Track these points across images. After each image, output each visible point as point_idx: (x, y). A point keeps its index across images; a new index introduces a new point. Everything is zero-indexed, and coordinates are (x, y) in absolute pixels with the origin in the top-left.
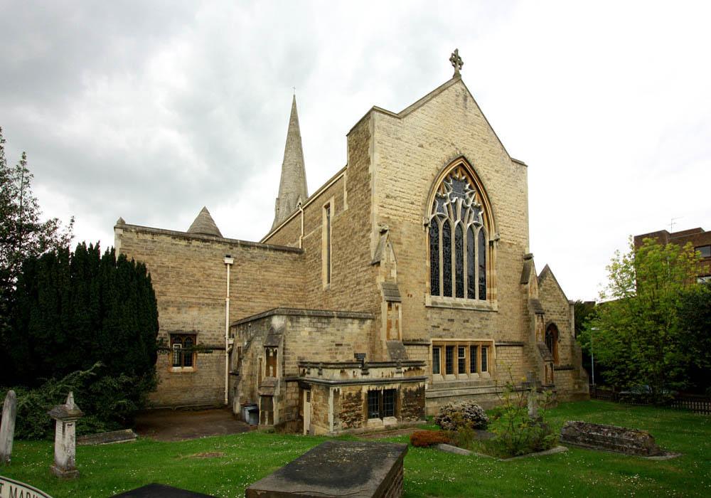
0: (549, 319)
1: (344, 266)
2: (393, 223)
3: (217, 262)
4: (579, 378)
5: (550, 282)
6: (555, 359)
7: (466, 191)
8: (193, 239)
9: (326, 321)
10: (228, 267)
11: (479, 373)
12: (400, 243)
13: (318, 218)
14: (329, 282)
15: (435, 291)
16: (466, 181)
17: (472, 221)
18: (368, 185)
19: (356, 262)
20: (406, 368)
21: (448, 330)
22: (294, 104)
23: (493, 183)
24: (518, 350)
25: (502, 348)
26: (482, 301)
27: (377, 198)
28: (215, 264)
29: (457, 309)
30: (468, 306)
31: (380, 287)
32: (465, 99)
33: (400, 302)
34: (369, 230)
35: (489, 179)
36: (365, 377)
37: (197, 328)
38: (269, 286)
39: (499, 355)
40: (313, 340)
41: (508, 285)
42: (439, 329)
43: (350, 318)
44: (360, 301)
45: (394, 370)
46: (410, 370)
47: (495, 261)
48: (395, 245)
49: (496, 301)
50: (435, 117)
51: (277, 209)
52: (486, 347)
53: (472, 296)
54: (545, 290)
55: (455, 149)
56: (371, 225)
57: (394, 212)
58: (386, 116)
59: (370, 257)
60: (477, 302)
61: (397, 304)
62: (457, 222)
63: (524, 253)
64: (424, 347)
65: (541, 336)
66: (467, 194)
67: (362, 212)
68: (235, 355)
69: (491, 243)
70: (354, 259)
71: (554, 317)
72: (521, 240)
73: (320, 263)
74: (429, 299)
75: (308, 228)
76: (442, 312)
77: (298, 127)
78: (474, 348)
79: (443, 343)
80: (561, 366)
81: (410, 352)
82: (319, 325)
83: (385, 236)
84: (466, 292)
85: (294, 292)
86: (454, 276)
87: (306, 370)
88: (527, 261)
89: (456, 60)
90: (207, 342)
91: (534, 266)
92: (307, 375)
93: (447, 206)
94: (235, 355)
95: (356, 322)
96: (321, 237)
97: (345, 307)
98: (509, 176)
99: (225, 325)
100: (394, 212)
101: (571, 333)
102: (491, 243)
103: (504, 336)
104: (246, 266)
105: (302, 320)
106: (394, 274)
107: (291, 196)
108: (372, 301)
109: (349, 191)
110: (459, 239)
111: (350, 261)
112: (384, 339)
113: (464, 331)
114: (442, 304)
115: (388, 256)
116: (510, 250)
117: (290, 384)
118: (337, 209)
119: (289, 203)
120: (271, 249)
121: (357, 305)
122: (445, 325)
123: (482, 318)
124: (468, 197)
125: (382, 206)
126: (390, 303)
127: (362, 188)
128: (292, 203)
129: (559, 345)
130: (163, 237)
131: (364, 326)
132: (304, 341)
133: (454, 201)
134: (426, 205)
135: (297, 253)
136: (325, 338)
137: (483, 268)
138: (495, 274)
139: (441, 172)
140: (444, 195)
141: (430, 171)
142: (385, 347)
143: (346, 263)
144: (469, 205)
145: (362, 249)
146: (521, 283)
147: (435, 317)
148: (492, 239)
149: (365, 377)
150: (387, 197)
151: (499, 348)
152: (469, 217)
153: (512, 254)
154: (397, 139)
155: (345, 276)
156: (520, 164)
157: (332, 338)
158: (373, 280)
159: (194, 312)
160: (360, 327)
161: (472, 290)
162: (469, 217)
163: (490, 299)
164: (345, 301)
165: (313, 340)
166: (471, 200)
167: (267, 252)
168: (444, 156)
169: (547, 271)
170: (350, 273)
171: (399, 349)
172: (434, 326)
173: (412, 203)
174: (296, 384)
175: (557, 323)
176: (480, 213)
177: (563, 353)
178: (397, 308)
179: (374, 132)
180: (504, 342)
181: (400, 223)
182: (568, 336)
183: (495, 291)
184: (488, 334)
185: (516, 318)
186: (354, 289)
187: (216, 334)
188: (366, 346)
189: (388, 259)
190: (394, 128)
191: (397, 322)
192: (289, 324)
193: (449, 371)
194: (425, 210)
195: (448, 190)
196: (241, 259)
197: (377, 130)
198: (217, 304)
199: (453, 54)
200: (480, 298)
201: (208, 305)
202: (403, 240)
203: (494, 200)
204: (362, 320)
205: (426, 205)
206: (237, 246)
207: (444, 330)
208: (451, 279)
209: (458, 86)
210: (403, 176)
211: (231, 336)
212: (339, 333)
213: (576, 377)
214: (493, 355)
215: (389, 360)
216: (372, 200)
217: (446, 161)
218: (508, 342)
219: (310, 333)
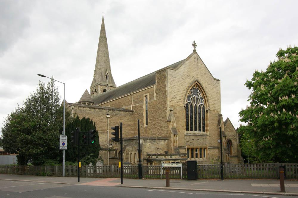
0: (228, 138)
1: (154, 120)
3: (104, 117)
4: (240, 160)
5: (229, 124)
6: (231, 153)
7: (198, 92)
8: (96, 108)
9: (154, 141)
10: (108, 118)
11: (203, 158)
12: (176, 114)
13: (141, 99)
14: (147, 124)
15: (187, 129)
16: (198, 89)
17: (200, 103)
18: (166, 94)
20: (182, 156)
21: (192, 143)
22: (103, 21)
23: (208, 89)
24: (217, 150)
25: (211, 149)
26: (203, 132)
27: (169, 98)
28: (104, 117)
29: (195, 135)
30: (199, 134)
31: (170, 129)
32: (198, 60)
33: (177, 134)
34: (166, 109)
35: (206, 88)
36: (171, 158)
39: (210, 152)
40: (150, 147)
41: (213, 126)
42: (189, 143)
43: (161, 139)
44: (162, 133)
45: (179, 156)
46: (183, 156)
47: (208, 117)
48: (175, 115)
49: (208, 132)
52: (205, 149)
53: (200, 130)
54: (227, 127)
55: (194, 78)
56: (167, 108)
57: (174, 103)
58: (171, 70)
59: (166, 118)
60: (202, 132)
61: (176, 135)
63: (219, 114)
64: (184, 149)
65: (225, 145)
66: (198, 93)
67: (163, 102)
69: (207, 111)
70: (159, 118)
71: (230, 137)
72: (218, 109)
74: (186, 132)
75: (136, 101)
76: (190, 137)
77: (105, 33)
78: (201, 149)
79: (190, 148)
80: (233, 156)
81: (181, 150)
82: (152, 142)
83: (172, 112)
84: (198, 129)
85: (130, 127)
86: (194, 123)
87: (150, 156)
88: (220, 117)
89: (194, 45)
91: (222, 119)
92: (151, 158)
93: (191, 99)
95: (163, 141)
96: (143, 107)
97: (155, 135)
98: (213, 86)
99: (107, 140)
100: (174, 103)
101: (237, 143)
102: (207, 111)
103: (212, 145)
104: (114, 118)
105: (147, 140)
106: (175, 124)
107: (103, 70)
109: (157, 94)
110: (196, 110)
111: (157, 118)
112: (172, 147)
113: (197, 143)
114: (189, 134)
115: (173, 119)
116: (214, 113)
117: (144, 161)
118: (150, 99)
120: (122, 111)
121: (161, 134)
122: (191, 141)
123: (204, 138)
125: (170, 102)
127: (163, 94)
129: (232, 148)
130: (86, 108)
131: (165, 142)
133: (194, 97)
134: (184, 99)
135: (131, 112)
136: (154, 146)
137: (204, 120)
138: (208, 122)
139: (189, 87)
141: (185, 88)
142: (173, 149)
143: (155, 119)
144: (199, 98)
145: (163, 115)
146: (218, 125)
147: (188, 139)
148: (207, 110)
149: (171, 158)
150: (172, 98)
151: (210, 149)
152: (199, 102)
153: (215, 114)
154: (175, 77)
156: (217, 80)
157: (156, 146)
158: (168, 127)
160: (164, 142)
161: (200, 128)
162: (199, 102)
163: (206, 131)
164: (155, 133)
165: (150, 147)
166: (200, 96)
167: (121, 112)
168: (190, 81)
169: (228, 120)
170: (157, 123)
171: (177, 150)
172: (188, 142)
173: (180, 99)
174: (146, 161)
175: (232, 140)
176: (203, 100)
177: (234, 151)
178: (176, 136)
179: (167, 76)
180: (212, 147)
182: (236, 145)
183: (208, 128)
184: (206, 144)
185: (216, 138)
186: (159, 129)
187: (104, 144)
188: (166, 149)
191: (176, 141)
192: (144, 142)
193: (192, 157)
194: (184, 101)
195: (192, 93)
196: (112, 115)
197: (168, 76)
199: (193, 43)
200: (203, 131)
201: (101, 133)
202: (177, 112)
203: (208, 95)
204: (165, 140)
205: (184, 99)
206: (110, 110)
207: (191, 143)
208: (193, 125)
209: (195, 55)
210: (177, 90)
212: (158, 144)
213: (239, 160)
214: (208, 152)
215: (175, 153)
216: (167, 99)
217: (191, 83)
218: (213, 147)
219: (150, 145)
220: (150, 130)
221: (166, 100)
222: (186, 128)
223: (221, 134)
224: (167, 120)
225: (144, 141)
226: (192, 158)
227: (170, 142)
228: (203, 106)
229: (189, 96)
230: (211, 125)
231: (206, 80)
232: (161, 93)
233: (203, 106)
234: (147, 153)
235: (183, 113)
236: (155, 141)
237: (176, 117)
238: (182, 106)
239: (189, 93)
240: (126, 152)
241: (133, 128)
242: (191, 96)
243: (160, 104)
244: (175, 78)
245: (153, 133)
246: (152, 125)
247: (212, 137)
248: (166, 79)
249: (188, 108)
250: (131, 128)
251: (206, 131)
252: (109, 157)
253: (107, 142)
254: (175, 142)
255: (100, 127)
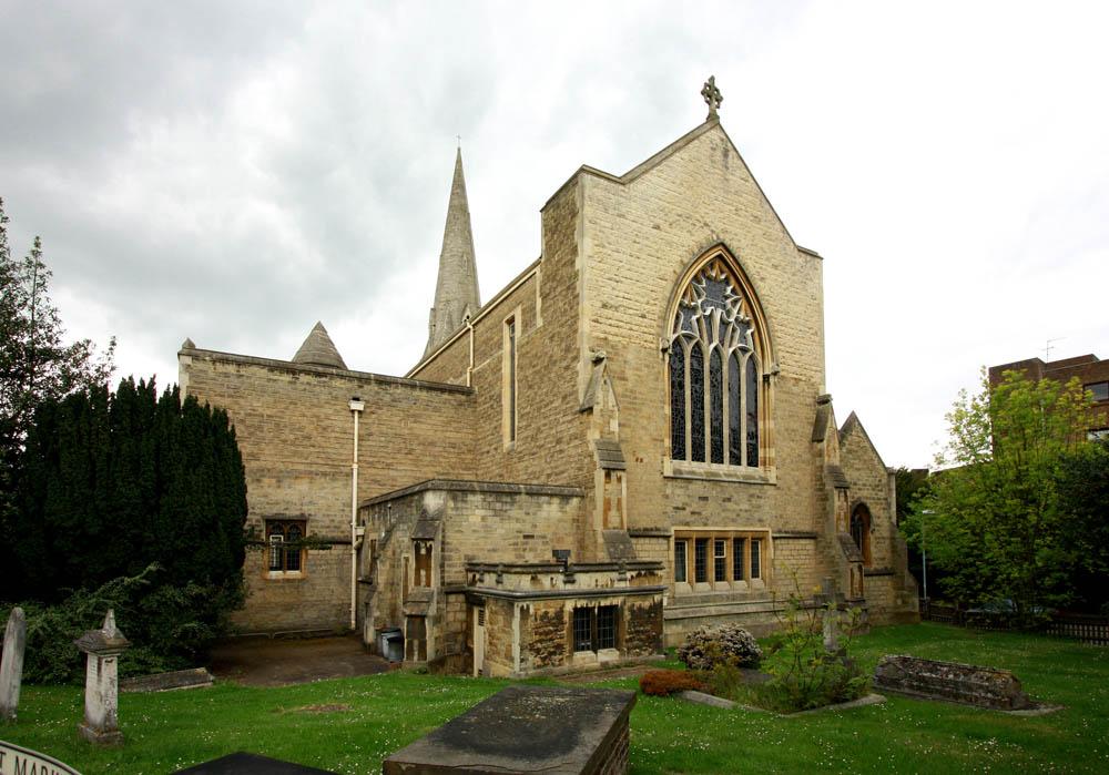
0: (856, 496)
2: (612, 347)
3: (338, 408)
5: (857, 439)
6: (865, 559)
7: (727, 298)
8: (301, 371)
9: (509, 500)
10: (356, 415)
11: (711, 583)
14: (513, 438)
15: (678, 453)
16: (727, 282)
17: (736, 345)
18: (575, 288)
19: (556, 408)
20: (634, 573)
21: (699, 513)
22: (459, 161)
23: (769, 285)
25: (783, 541)
26: (751, 469)
27: (588, 307)
29: (713, 480)
31: (592, 447)
33: (624, 470)
34: (576, 358)
35: (762, 279)
36: (569, 587)
37: (307, 510)
38: (419, 444)
39: (778, 552)
40: (487, 529)
44: (561, 469)
45: (615, 575)
46: (639, 575)
47: (772, 405)
48: (617, 382)
49: (773, 468)
50: (678, 182)
51: (433, 326)
52: (757, 540)
53: (736, 460)
54: (849, 452)
59: (577, 399)
60: (743, 469)
61: (619, 473)
62: (713, 346)
63: (817, 393)
66: (728, 301)
68: (367, 552)
69: (766, 378)
70: (552, 402)
71: (865, 494)
73: (498, 409)
74: (670, 466)
75: (480, 354)
76: (690, 486)
77: (465, 197)
78: (739, 542)
80: (876, 569)
82: (498, 506)
84: (726, 454)
86: (708, 430)
87: (478, 576)
88: (821, 407)
89: (711, 93)
90: (323, 533)
91: (833, 413)
92: (479, 584)
93: (698, 320)
94: (367, 552)
95: (556, 501)
96: (501, 369)
97: (538, 478)
98: (794, 275)
101: (890, 518)
102: (766, 378)
104: (384, 414)
105: (470, 497)
106: (614, 426)
107: (455, 306)
108: (580, 469)
109: (545, 297)
111: (546, 406)
112: (599, 528)
113: (723, 514)
115: (604, 399)
116: (795, 389)
117: (452, 598)
118: (526, 325)
119: (450, 316)
120: (422, 387)
121: (556, 475)
122: (695, 507)
123: (752, 496)
124: (729, 306)
125: (596, 321)
126: (608, 472)
127: (564, 293)
128: (455, 317)
131: (568, 508)
132: (474, 531)
133: (708, 313)
134: (664, 319)
136: (507, 525)
137: (753, 416)
138: (772, 426)
139: (687, 267)
140: (693, 304)
141: (671, 267)
142: (600, 540)
143: (539, 409)
144: (732, 320)
145: (565, 388)
147: (678, 494)
148: (767, 372)
149: (569, 587)
150: (604, 306)
151: (778, 542)
152: (732, 337)
154: (620, 216)
155: (539, 429)
157: (518, 526)
158: (581, 436)
159: (303, 486)
162: (732, 337)
163: (764, 464)
165: (487, 529)
166: (735, 311)
167: (417, 393)
168: (692, 243)
169: (853, 421)
170: (545, 425)
171: (623, 543)
172: (677, 508)
173: (643, 316)
174: (461, 598)
175: (869, 503)
176: (749, 332)
177: (878, 550)
178: (619, 480)
179: (583, 206)
180: (786, 532)
181: (624, 347)
182: (886, 524)
183: (772, 453)
184: (760, 521)
185: (805, 494)
187: (337, 519)
189: (606, 403)
190: (614, 199)
191: (619, 501)
193: (701, 577)
194: (663, 328)
195: (699, 296)
197: (587, 202)
198: (338, 473)
199: (706, 85)
200: (749, 464)
201: (325, 474)
202: (629, 373)
203: (770, 310)
204: (566, 498)
205: (664, 319)
206: (370, 384)
207: (693, 513)
208: (703, 435)
209: (714, 134)
210: (628, 274)
211: (360, 523)
213: (899, 587)
214: (768, 553)
215: (607, 561)
217: (696, 251)
218: (792, 533)
219: (483, 518)
220: (520, 459)
221: (578, 315)
222: (674, 448)
223: (829, 481)
224: (578, 408)
225: (455, 499)
226: (698, 581)
227: (589, 508)
228: (749, 354)
229: (688, 309)
230: (784, 439)
231: (762, 248)
232: (559, 289)
233: (749, 354)
234: (466, 556)
235: (657, 379)
236: (513, 503)
237: (624, 396)
238: (653, 346)
239: (685, 294)
240: (389, 553)
241: (471, 457)
242: (694, 309)
243: (556, 338)
244: (618, 219)
245: (531, 474)
246: (527, 437)
247: (789, 489)
248: (578, 221)
249: (682, 361)
250: (463, 460)
251: (764, 464)
252: (358, 574)
253: (351, 511)
254: (614, 503)
255: (321, 450)
